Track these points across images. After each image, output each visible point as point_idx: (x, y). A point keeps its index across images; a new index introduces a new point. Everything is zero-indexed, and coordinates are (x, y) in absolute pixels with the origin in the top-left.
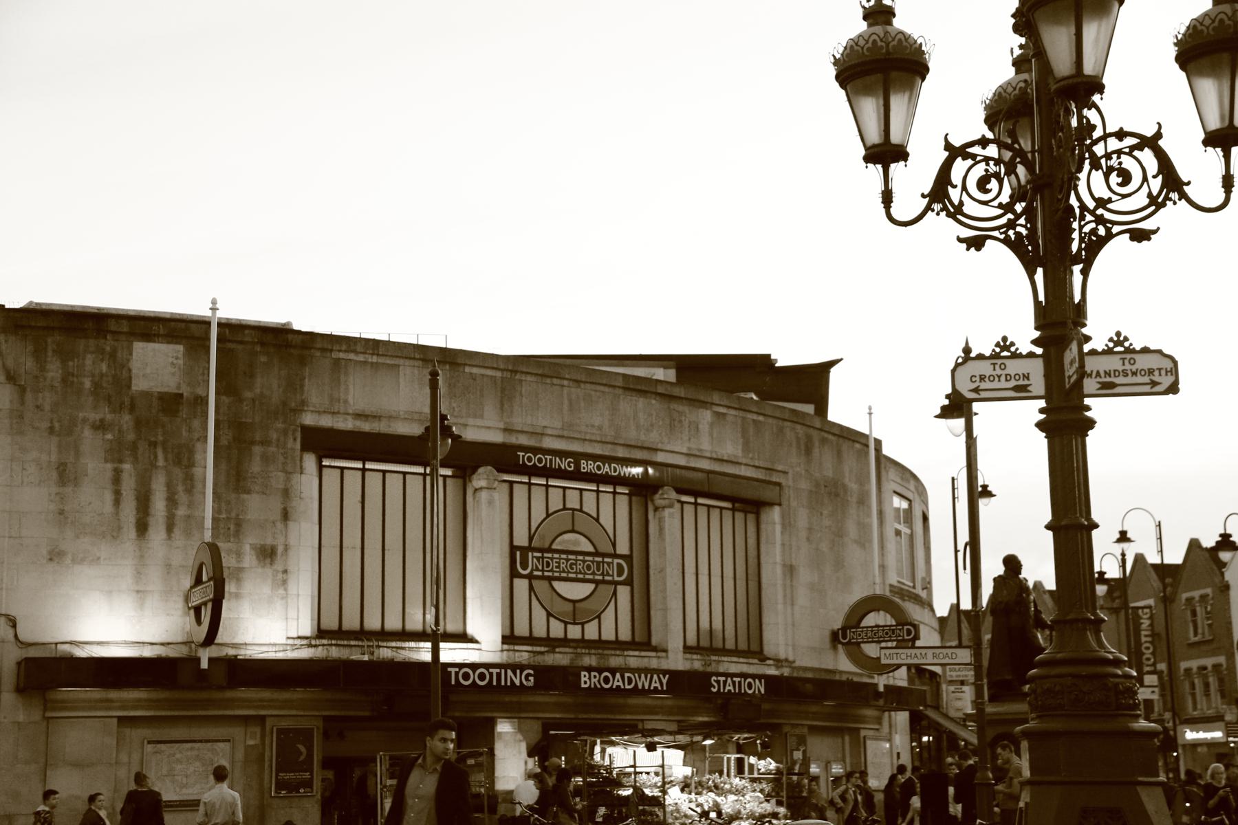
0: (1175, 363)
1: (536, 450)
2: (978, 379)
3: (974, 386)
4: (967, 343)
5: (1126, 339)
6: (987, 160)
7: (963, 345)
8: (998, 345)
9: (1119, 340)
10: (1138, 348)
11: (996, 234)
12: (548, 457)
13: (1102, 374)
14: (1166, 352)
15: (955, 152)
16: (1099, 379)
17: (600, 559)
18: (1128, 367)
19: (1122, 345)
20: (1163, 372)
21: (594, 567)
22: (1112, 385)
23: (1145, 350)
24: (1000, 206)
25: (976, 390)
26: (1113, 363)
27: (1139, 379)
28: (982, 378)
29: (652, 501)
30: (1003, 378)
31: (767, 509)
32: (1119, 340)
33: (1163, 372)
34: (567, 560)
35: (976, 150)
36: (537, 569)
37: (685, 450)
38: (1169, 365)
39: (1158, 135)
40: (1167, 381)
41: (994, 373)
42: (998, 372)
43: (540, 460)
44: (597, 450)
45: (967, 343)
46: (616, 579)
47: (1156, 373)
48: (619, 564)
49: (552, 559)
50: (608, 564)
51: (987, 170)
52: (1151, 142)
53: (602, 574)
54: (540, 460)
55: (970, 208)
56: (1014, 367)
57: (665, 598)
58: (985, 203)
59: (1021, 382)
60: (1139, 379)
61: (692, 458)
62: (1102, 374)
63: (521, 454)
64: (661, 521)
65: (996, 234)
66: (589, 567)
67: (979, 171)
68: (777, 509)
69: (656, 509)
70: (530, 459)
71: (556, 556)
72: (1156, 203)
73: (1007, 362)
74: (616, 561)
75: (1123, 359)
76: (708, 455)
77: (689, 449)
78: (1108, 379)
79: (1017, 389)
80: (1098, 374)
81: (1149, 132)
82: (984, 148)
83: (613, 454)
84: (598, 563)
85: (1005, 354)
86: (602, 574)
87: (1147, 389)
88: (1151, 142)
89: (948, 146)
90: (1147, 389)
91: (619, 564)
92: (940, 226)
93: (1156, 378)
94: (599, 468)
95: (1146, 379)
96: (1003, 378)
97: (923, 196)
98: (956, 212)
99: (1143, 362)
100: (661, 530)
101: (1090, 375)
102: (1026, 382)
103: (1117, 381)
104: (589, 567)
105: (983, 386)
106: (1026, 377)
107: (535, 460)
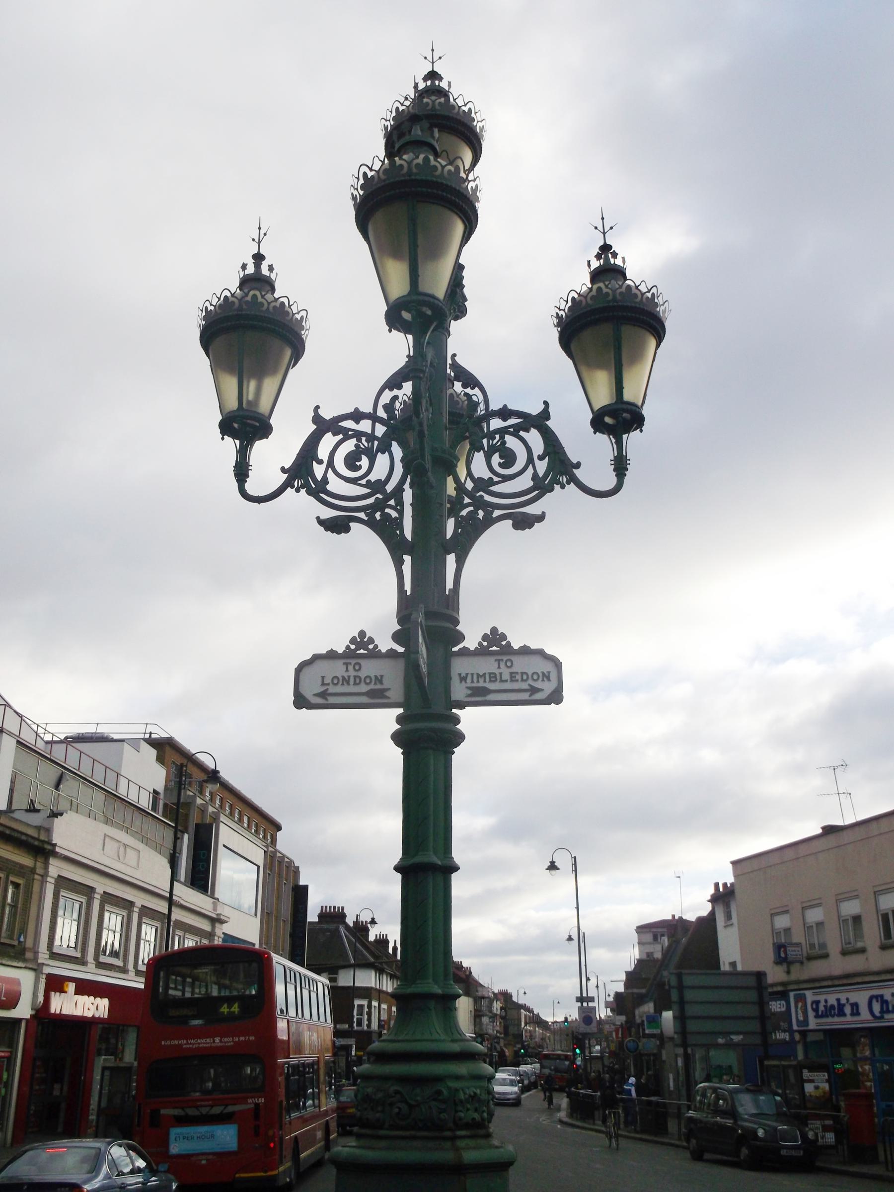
0: (557, 664)
5: (371, 641)
6: (358, 435)
8: (353, 641)
9: (495, 637)
10: (516, 646)
11: (362, 515)
15: (323, 426)
18: (352, 673)
19: (367, 649)
22: (484, 691)
23: (525, 651)
24: (369, 485)
25: (323, 695)
26: (487, 665)
32: (495, 637)
35: (349, 424)
39: (545, 414)
40: (548, 688)
51: (357, 446)
52: (539, 421)
55: (335, 485)
56: (370, 668)
58: (354, 481)
59: (372, 686)
65: (362, 515)
67: (350, 445)
72: (541, 487)
73: (363, 662)
78: (481, 684)
79: (371, 694)
81: (535, 409)
82: (357, 422)
88: (539, 421)
89: (317, 418)
90: (525, 696)
92: (298, 501)
97: (223, 439)
98: (318, 490)
102: (379, 686)
103: (492, 686)
105: (332, 689)
106: (379, 680)
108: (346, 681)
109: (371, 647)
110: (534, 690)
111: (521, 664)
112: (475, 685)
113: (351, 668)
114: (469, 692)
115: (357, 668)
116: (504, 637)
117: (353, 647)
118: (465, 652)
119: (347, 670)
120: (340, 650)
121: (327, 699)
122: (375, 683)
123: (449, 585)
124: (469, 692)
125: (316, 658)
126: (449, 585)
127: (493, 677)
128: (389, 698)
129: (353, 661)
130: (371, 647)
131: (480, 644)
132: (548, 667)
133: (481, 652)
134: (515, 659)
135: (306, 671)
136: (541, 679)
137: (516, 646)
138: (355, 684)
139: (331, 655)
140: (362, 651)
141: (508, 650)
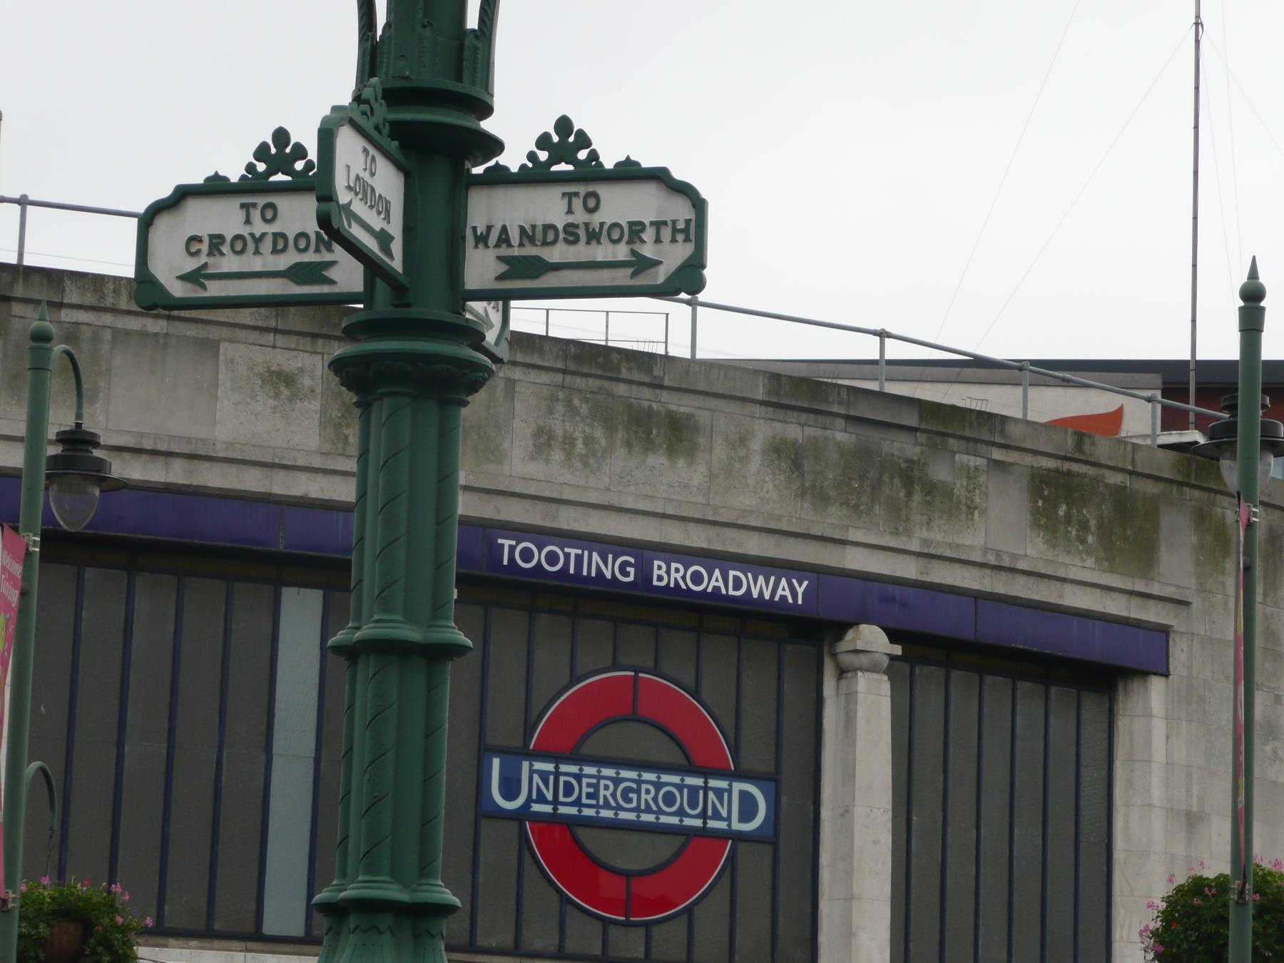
0: (699, 205)
1: (542, 535)
2: (205, 247)
3: (191, 265)
4: (1253, 274)
5: (583, 140)
7: (1243, 278)
8: (262, 152)
9: (565, 139)
12: (574, 552)
13: (515, 237)
14: (678, 174)
16: (504, 251)
17: (699, 782)
19: (572, 160)
20: (666, 233)
21: (682, 799)
22: (537, 267)
23: (629, 172)
25: (194, 277)
26: (547, 207)
27: (603, 252)
28: (216, 242)
29: (834, 655)
30: (267, 245)
31: (1136, 685)
32: (565, 139)
33: (666, 233)
34: (617, 781)
36: (541, 799)
37: (915, 546)
38: (680, 211)
40: (674, 255)
41: (244, 231)
42: (259, 227)
43: (552, 558)
44: (697, 538)
45: (1253, 274)
46: (737, 826)
47: (648, 235)
48: (744, 795)
49: (578, 777)
50: (719, 792)
53: (703, 815)
54: (552, 558)
57: (849, 874)
59: (310, 257)
60: (603, 252)
61: (935, 564)
62: (515, 237)
63: (507, 543)
64: (850, 699)
66: (669, 799)
68: (1156, 683)
69: (842, 672)
70: (527, 555)
71: (589, 770)
73: (281, 202)
74: (738, 786)
75: (570, 196)
76: (977, 557)
77: (925, 542)
78: (530, 251)
80: (504, 239)
83: (548, 524)
84: (693, 790)
85: (280, 177)
86: (703, 815)
87: (622, 277)
90: (622, 277)
91: (744, 795)
93: (648, 251)
94: (697, 578)
95: (621, 252)
96: (267, 245)
99: (619, 205)
100: (849, 720)
101: (482, 240)
103: (556, 254)
104: (669, 799)
107: (539, 557)
108: (571, 233)
109: (582, 155)
110: (641, 264)
111: (619, 205)
112: (516, 252)
113: (256, 215)
114: (503, 268)
115: (269, 215)
116: (583, 140)
117: (261, 167)
118: (500, 177)
119: (248, 221)
120: (234, 174)
121: (204, 287)
122: (317, 250)
123: (472, 21)
124: (503, 268)
125: (183, 194)
126: (472, 21)
127: (548, 234)
128: (332, 282)
129: (261, 201)
130: (582, 155)
131: (250, 168)
132: (680, 211)
133: (534, 176)
134: (607, 193)
135: (163, 224)
136: (313, 246)
137: (608, 162)
138: (275, 251)
139: (216, 187)
140: (280, 177)
141: (592, 173)
